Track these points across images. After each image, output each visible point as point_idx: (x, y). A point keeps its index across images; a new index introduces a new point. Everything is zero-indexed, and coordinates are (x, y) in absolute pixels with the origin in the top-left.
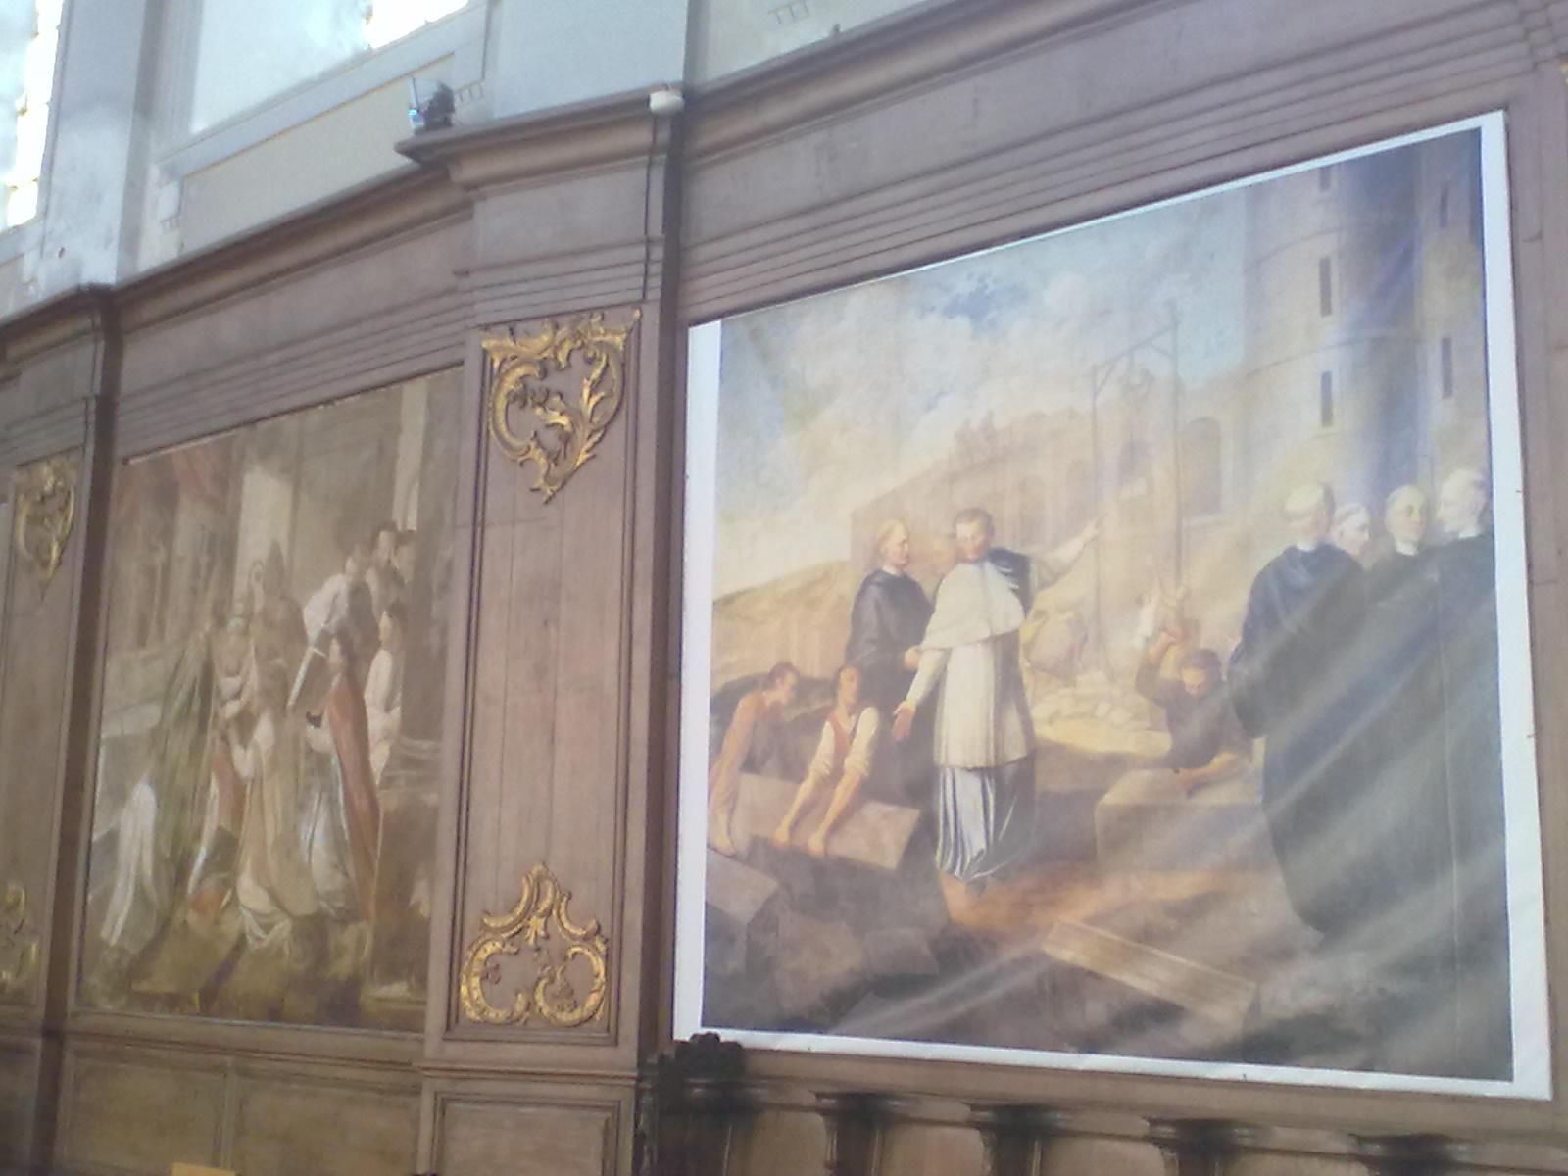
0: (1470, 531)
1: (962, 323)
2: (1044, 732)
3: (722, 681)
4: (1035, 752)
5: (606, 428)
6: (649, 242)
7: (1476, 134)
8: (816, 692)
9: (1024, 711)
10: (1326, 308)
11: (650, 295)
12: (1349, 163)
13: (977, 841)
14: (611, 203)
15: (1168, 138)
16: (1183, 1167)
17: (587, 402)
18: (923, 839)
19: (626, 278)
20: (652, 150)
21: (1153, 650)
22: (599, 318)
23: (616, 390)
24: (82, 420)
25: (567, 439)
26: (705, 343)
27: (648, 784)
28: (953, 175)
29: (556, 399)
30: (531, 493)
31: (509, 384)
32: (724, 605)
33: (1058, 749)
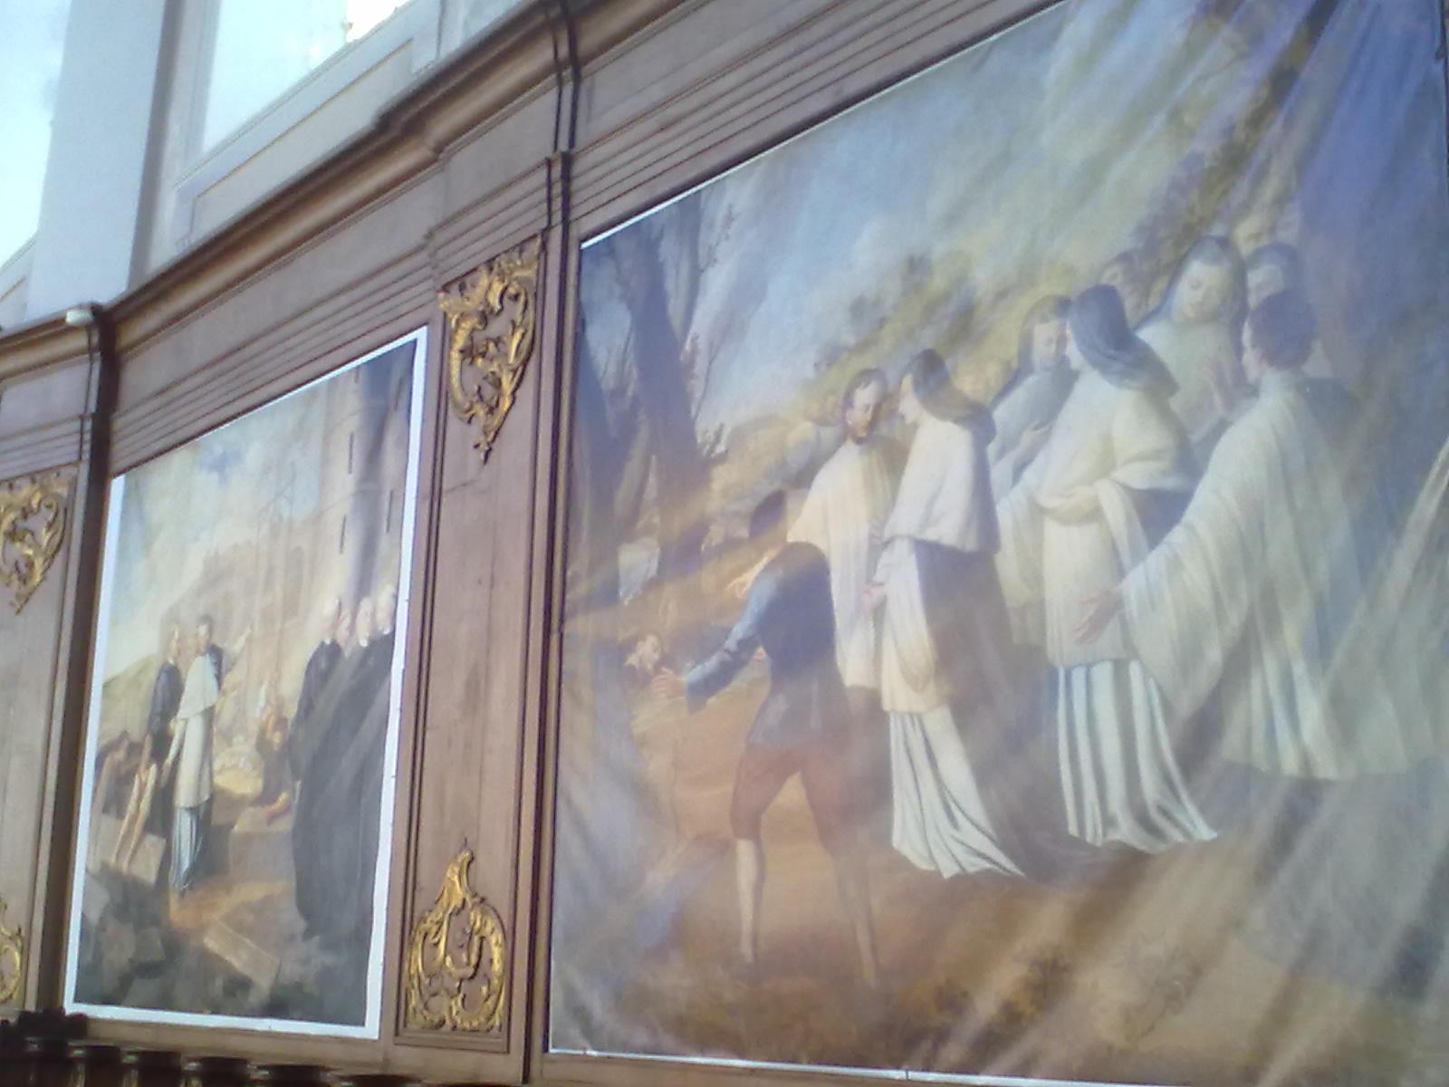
0: (971, 545)
1: (215, 476)
2: (220, 781)
3: (104, 742)
4: (215, 794)
5: (53, 556)
6: (82, 418)
7: (415, 342)
8: (134, 749)
9: (211, 765)
10: (350, 472)
11: (84, 458)
12: (368, 363)
13: (186, 864)
14: (67, 388)
15: (404, 290)
16: (204, 1085)
17: (45, 537)
18: (167, 858)
19: (67, 448)
20: (90, 350)
21: (264, 718)
22: (55, 475)
23: (61, 529)
24: (77, 437)
25: (30, 565)
26: (117, 486)
27: (380, 812)
28: (218, 368)
29: (28, 536)
30: (487, 464)
31: (460, 340)
32: (106, 686)
33: (223, 791)
